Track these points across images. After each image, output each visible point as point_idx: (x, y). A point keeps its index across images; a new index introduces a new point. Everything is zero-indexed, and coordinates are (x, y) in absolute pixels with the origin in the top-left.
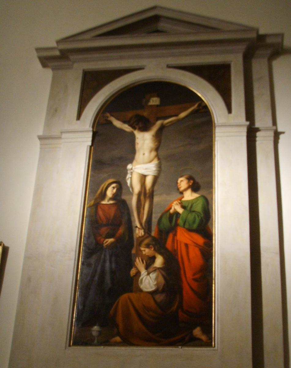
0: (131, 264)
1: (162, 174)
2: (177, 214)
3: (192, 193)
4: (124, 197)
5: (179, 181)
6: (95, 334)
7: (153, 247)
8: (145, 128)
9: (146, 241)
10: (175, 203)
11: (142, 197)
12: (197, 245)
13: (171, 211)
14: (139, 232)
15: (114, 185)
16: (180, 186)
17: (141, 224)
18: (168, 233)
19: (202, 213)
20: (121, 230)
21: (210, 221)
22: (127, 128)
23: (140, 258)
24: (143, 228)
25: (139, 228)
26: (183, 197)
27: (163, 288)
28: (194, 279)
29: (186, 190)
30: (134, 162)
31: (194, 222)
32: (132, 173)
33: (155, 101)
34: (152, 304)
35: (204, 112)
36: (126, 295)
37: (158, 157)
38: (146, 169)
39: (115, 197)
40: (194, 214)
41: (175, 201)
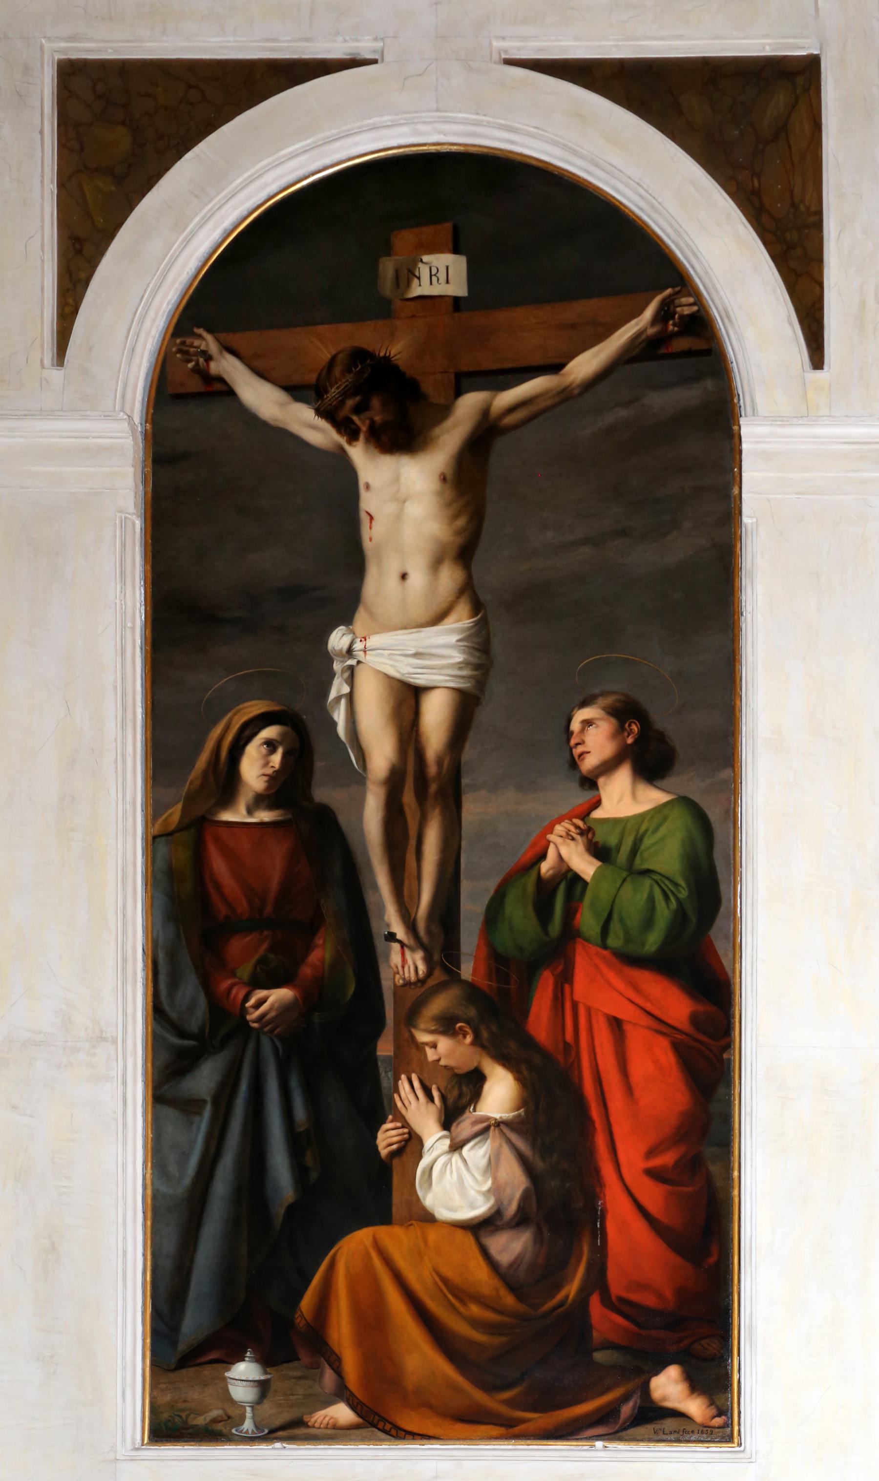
0: (376, 1108)
1: (497, 688)
2: (571, 880)
3: (634, 782)
4: (322, 794)
5: (575, 726)
6: (242, 1393)
8: (401, 437)
9: (438, 1004)
10: (559, 829)
11: (409, 798)
12: (662, 1026)
13: (546, 867)
14: (404, 964)
15: (270, 732)
16: (580, 749)
17: (411, 926)
18: (531, 969)
19: (682, 882)
20: (323, 952)
22: (313, 427)
23: (414, 1077)
24: (420, 944)
25: (403, 945)
26: (597, 803)
27: (521, 1209)
28: (650, 1173)
29: (608, 767)
30: (361, 617)
31: (648, 922)
33: (442, 274)
34: (480, 1275)
35: (691, 344)
36: (355, 1246)
38: (417, 655)
39: (286, 789)
40: (647, 882)
41: (559, 820)
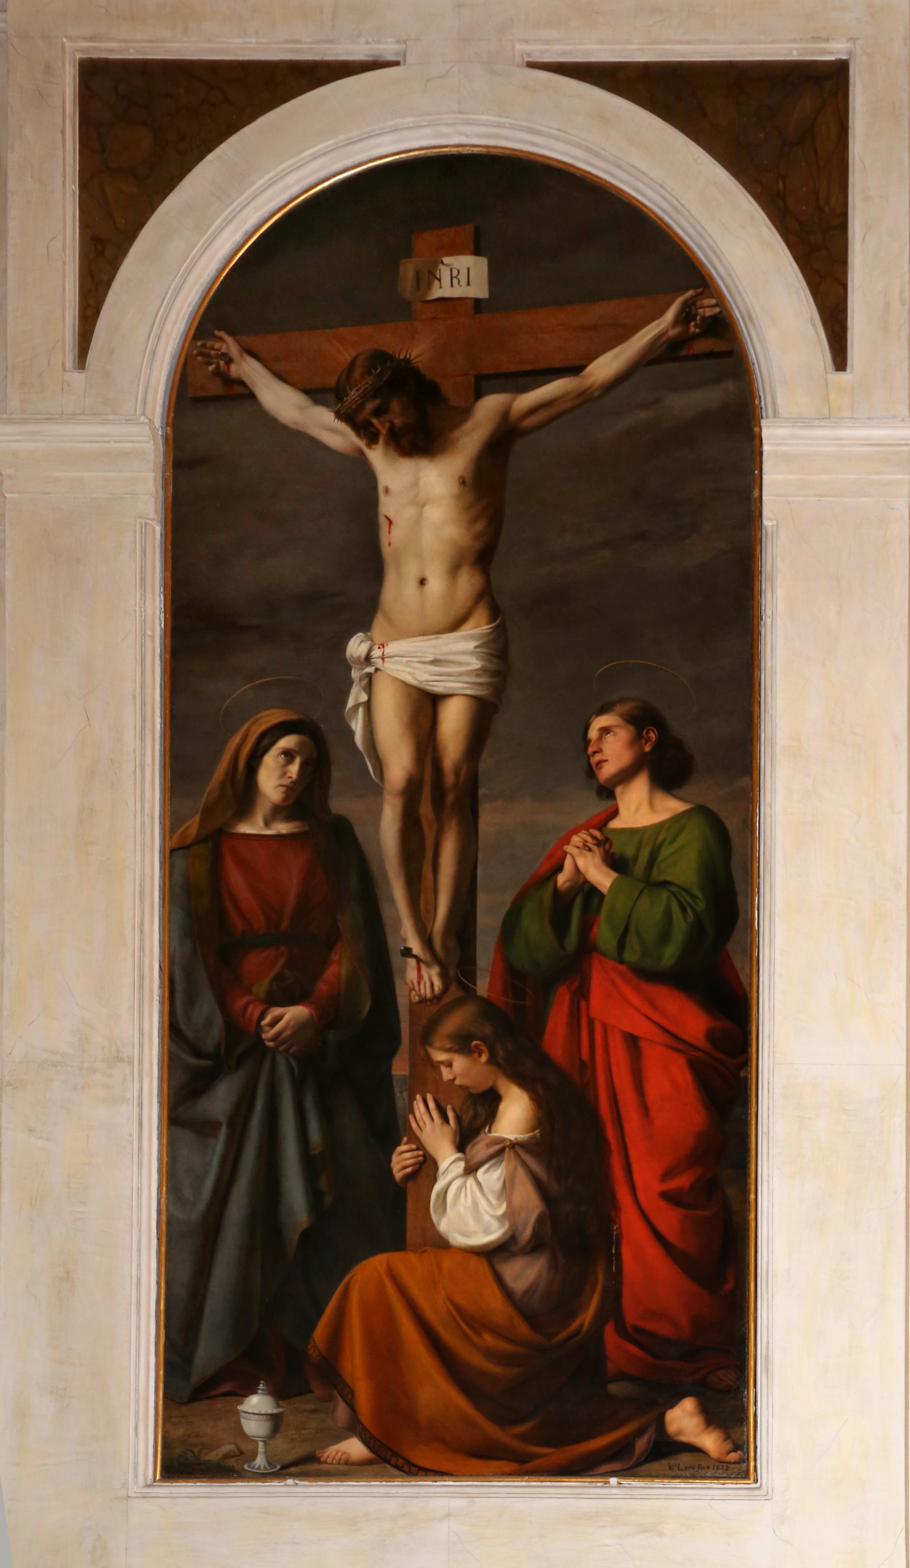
0: (390, 1130)
2: (587, 891)
4: (339, 804)
5: (593, 734)
6: (254, 1427)
7: (484, 1048)
8: (420, 439)
9: (454, 1022)
11: (426, 808)
13: (562, 879)
14: (419, 980)
15: (287, 742)
17: (427, 941)
19: (699, 894)
20: (340, 967)
21: (736, 935)
23: (429, 1097)
24: (436, 959)
25: (416, 957)
26: (615, 813)
27: (536, 1234)
28: (666, 1196)
29: (626, 776)
30: (379, 623)
31: (665, 936)
32: (369, 683)
33: (463, 276)
34: (494, 1304)
35: (713, 345)
36: (376, 1263)
37: (488, 598)
38: (435, 662)
39: (304, 800)
40: (664, 894)
41: (576, 831)
